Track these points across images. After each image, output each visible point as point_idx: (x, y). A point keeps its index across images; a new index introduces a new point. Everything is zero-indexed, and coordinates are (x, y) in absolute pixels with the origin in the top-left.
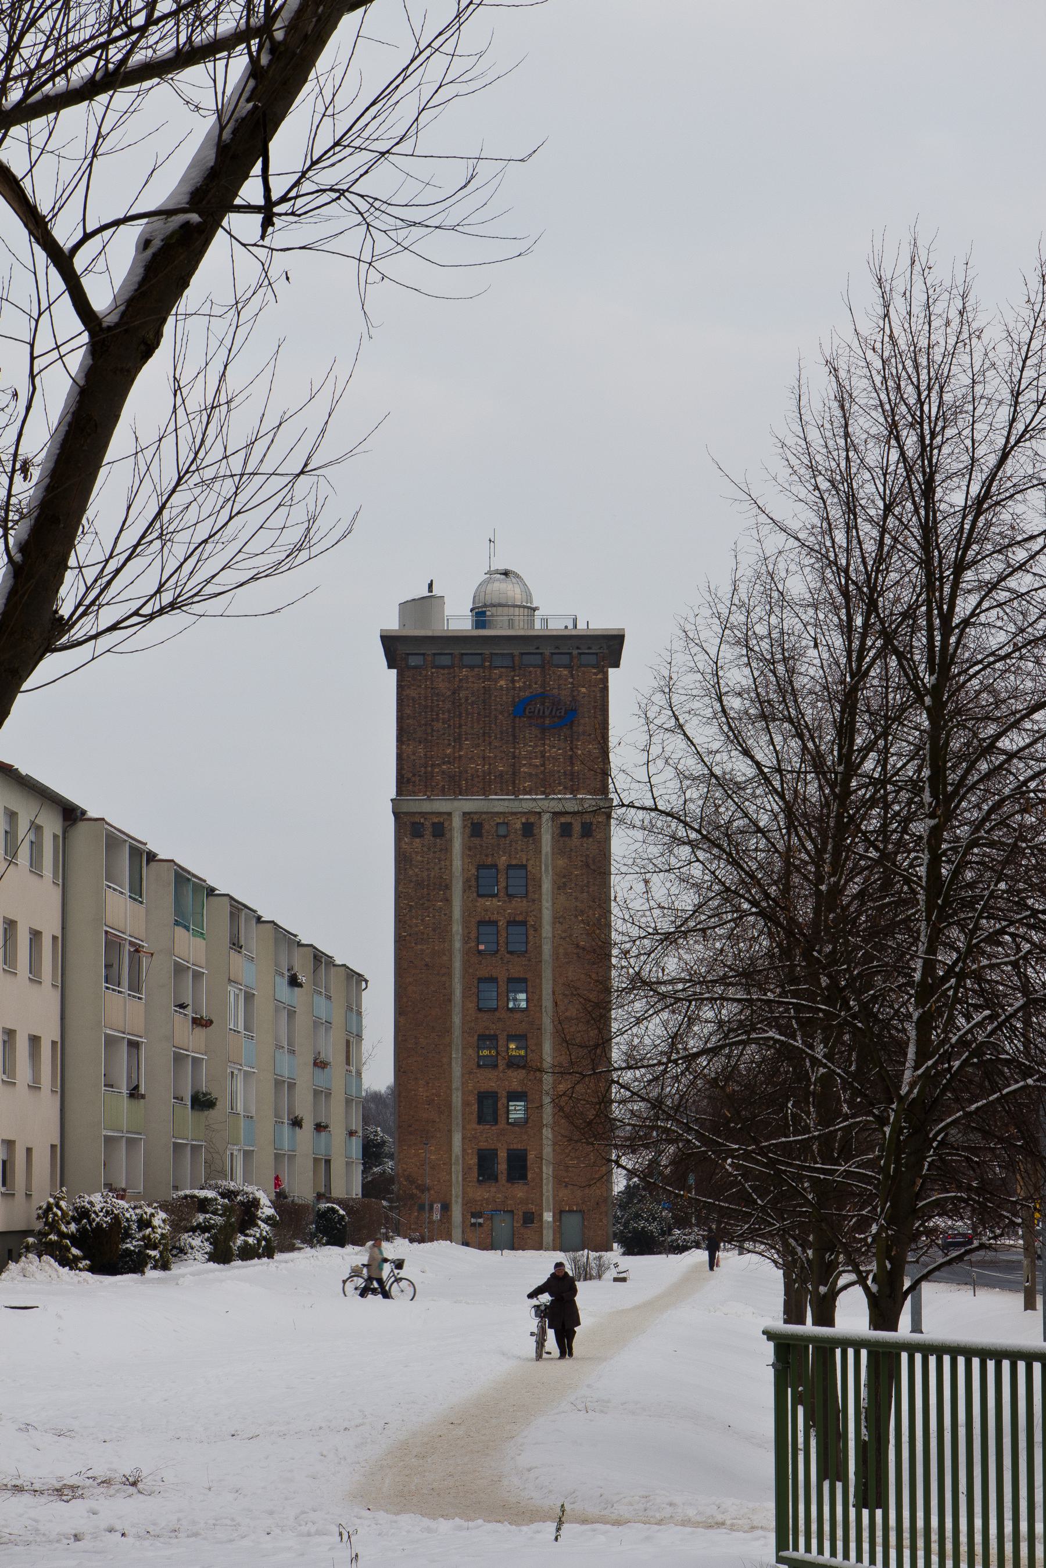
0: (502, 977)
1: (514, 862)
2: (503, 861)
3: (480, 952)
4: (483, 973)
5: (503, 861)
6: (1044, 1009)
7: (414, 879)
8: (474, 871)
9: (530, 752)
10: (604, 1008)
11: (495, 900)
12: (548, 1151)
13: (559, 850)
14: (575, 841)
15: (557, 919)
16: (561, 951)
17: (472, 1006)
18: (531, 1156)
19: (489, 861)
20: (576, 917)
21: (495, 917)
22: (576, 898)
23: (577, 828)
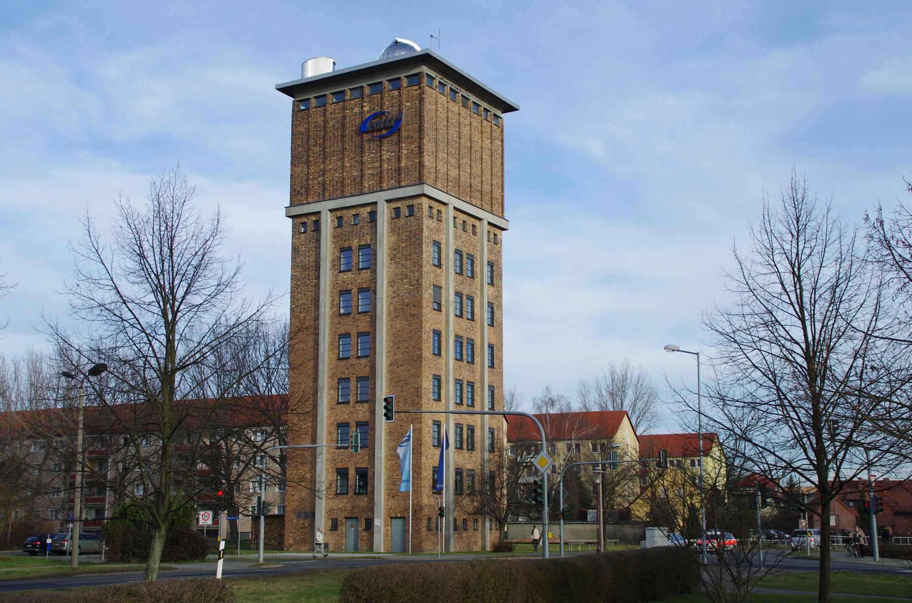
0: (354, 333)
1: (362, 243)
2: (355, 243)
3: (340, 315)
4: (342, 330)
5: (355, 243)
6: (3, 464)
7: (300, 264)
8: (337, 254)
9: (373, 158)
10: (39, 415)
11: (350, 273)
12: (21, 569)
13: (393, 230)
14: (402, 221)
15: (392, 283)
16: (392, 308)
17: (334, 357)
18: (370, 473)
19: (346, 245)
20: (402, 280)
21: (349, 287)
22: (403, 265)
23: (405, 211)
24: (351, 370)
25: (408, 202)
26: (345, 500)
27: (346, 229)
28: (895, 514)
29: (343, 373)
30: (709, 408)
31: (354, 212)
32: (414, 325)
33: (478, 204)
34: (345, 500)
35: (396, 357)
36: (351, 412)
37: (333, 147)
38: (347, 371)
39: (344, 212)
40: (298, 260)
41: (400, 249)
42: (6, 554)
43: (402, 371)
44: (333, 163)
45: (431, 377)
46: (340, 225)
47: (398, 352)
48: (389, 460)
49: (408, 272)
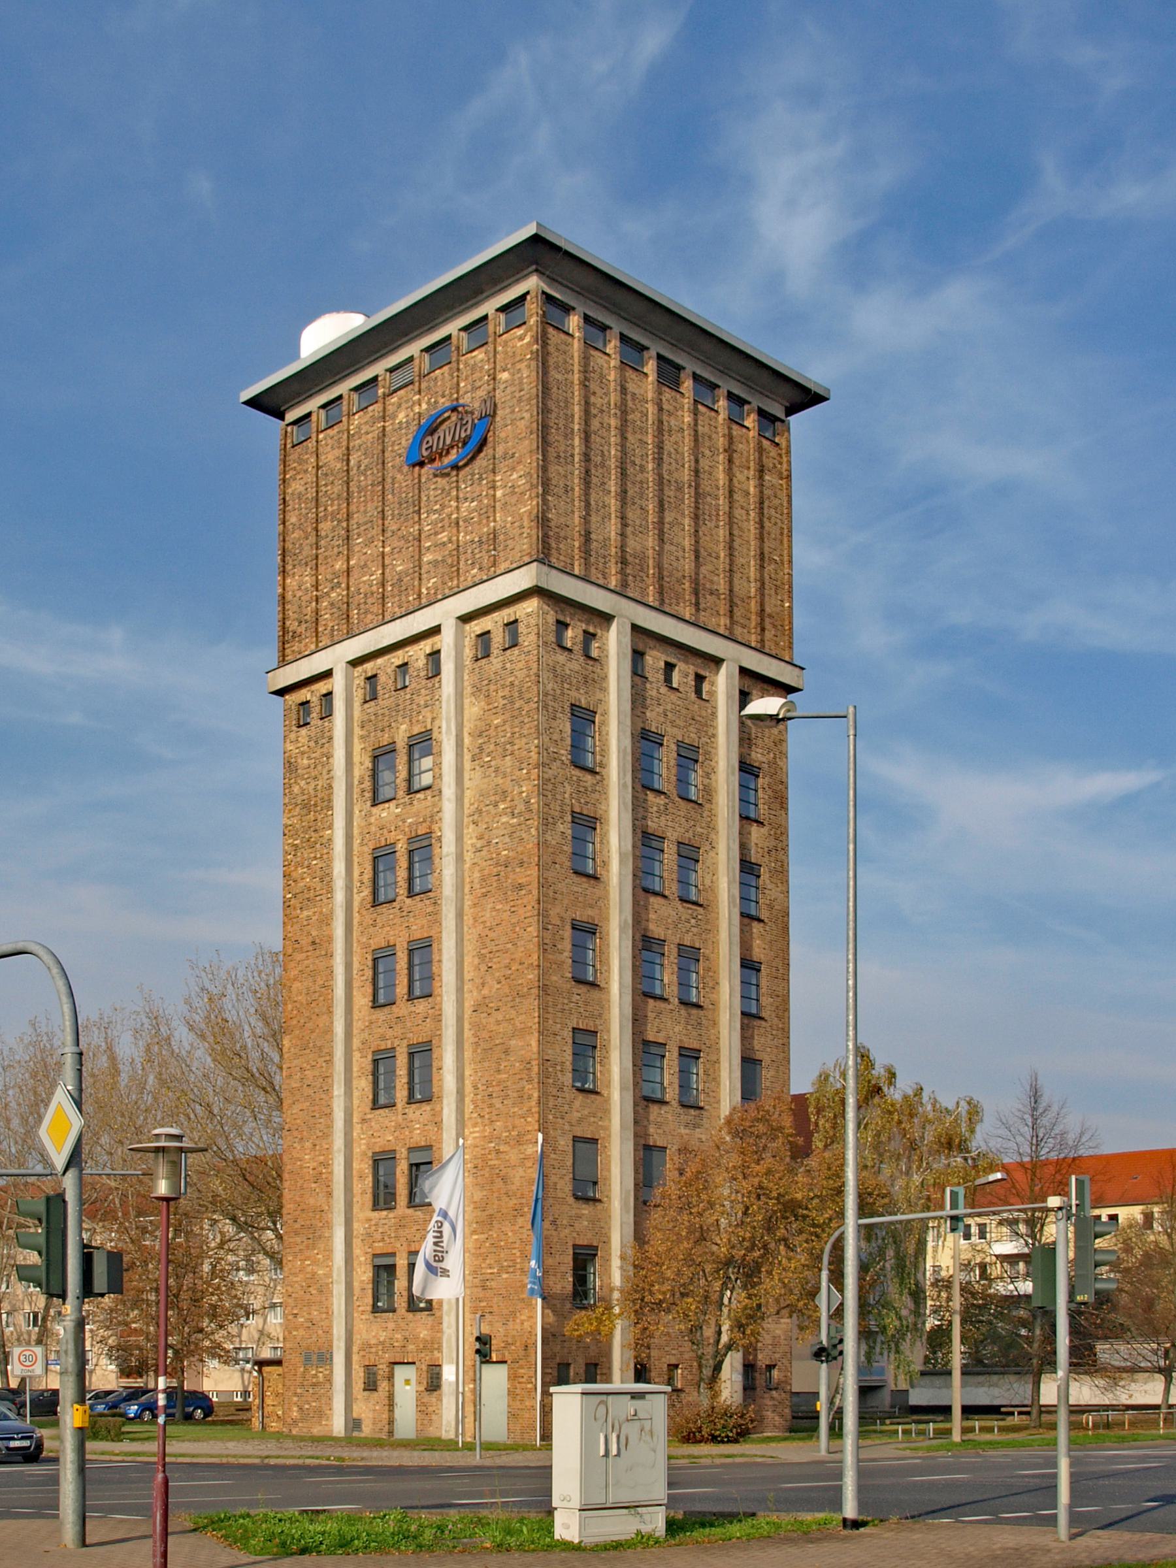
14: (495, 661)
20: (496, 806)
23: (498, 638)
24: (398, 1031)
25: (506, 614)
26: (391, 1325)
27: (386, 699)
28: (374, 698)
29: (383, 1038)
30: (478, 723)
31: (397, 658)
32: (521, 911)
33: (753, 640)
34: (391, 1325)
35: (485, 992)
36: (399, 1127)
37: (365, 510)
38: (390, 1033)
39: (380, 661)
40: (296, 789)
41: (492, 732)
42: (7, 1514)
43: (498, 1023)
44: (364, 550)
45: (567, 1034)
46: (372, 696)
47: (488, 979)
48: (474, 1232)
49: (507, 784)
